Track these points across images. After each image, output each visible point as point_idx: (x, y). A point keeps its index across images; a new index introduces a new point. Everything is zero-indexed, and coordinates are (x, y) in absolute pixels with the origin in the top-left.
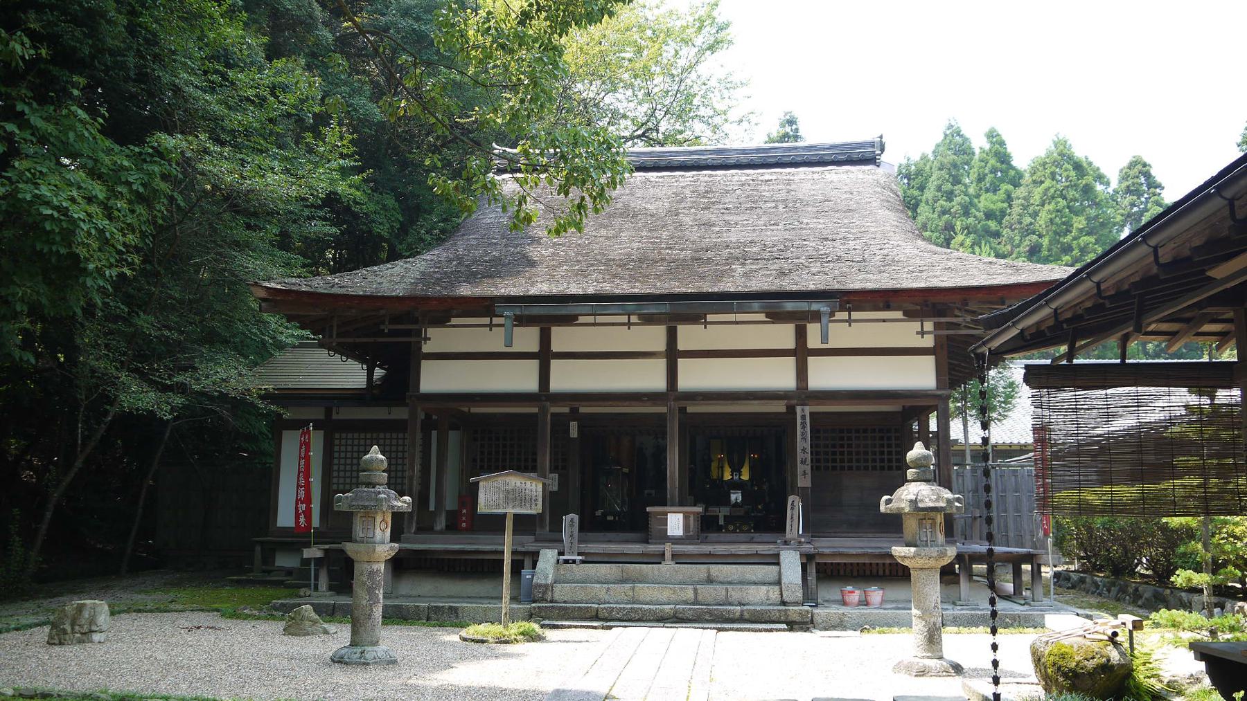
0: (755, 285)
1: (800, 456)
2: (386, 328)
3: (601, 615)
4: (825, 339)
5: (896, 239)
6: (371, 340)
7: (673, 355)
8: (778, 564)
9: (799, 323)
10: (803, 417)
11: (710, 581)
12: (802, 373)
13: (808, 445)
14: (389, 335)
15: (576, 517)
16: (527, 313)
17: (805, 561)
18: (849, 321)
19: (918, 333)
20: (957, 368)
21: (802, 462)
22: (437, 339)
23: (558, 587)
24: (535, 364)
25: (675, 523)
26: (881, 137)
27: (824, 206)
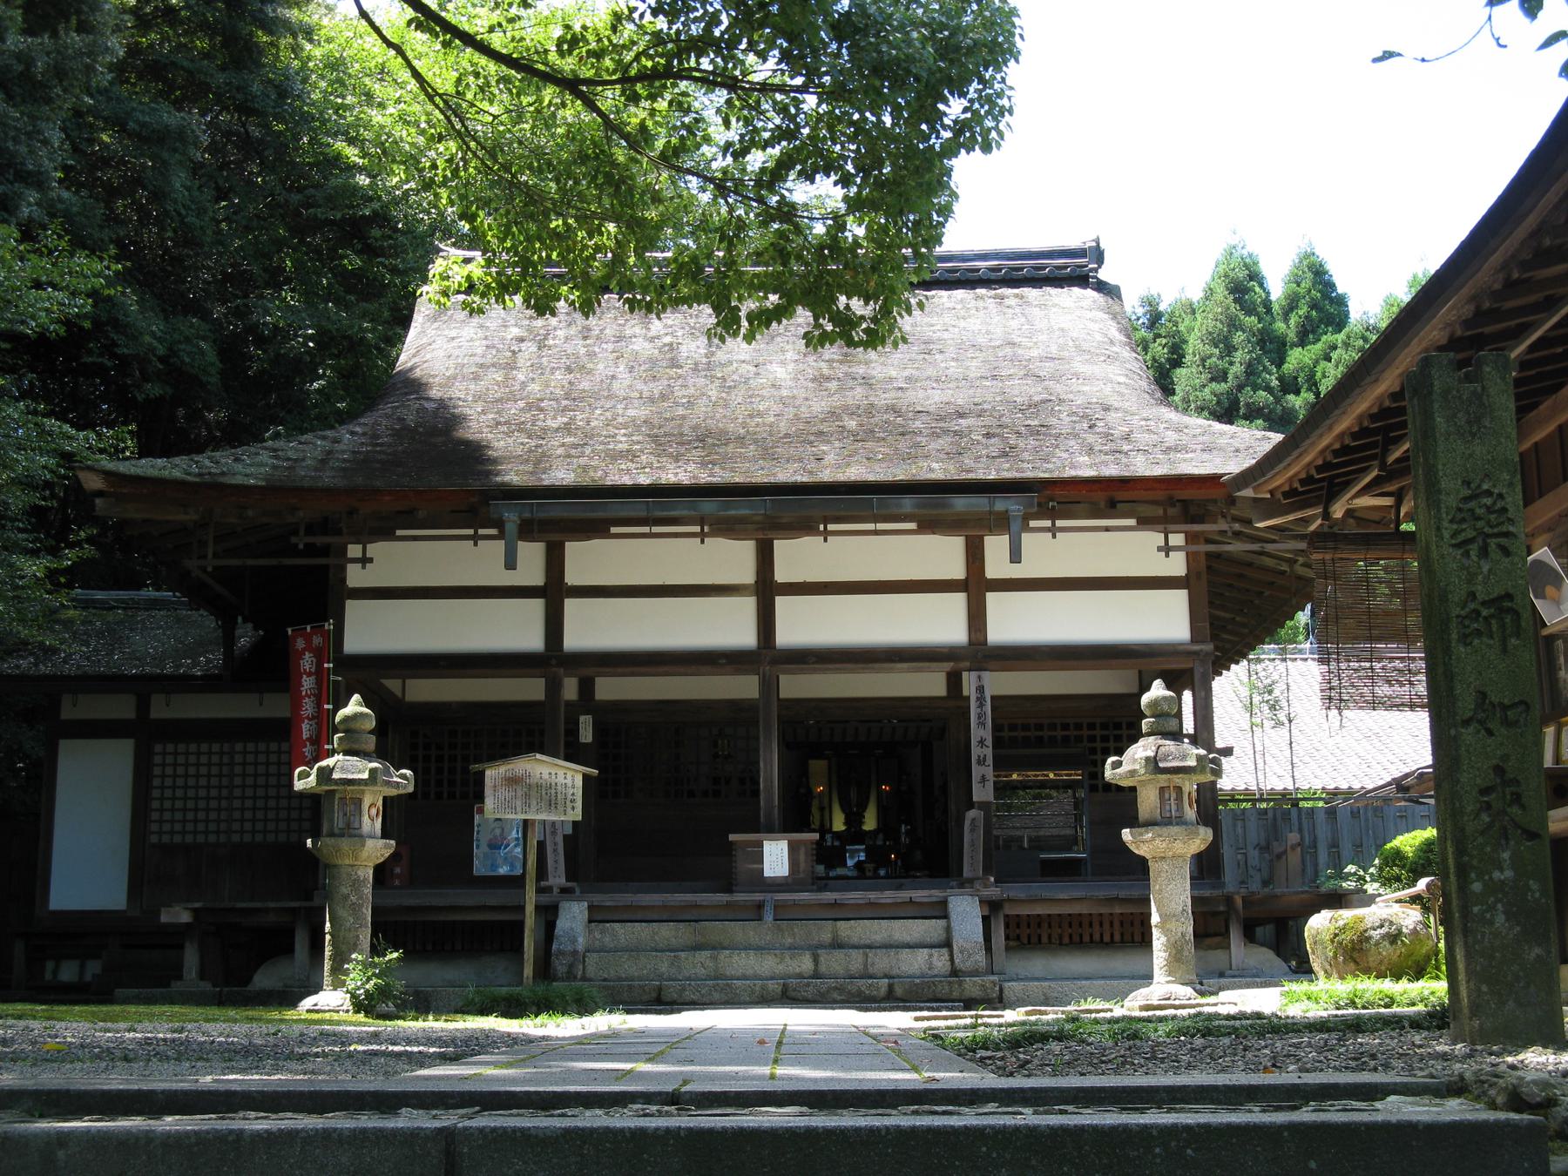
1: (976, 751)
2: (301, 542)
4: (1015, 557)
6: (273, 562)
7: (766, 590)
8: (946, 916)
11: (837, 945)
12: (977, 618)
16: (542, 515)
17: (986, 913)
18: (1053, 531)
19: (1159, 549)
20: (1230, 627)
21: (979, 762)
23: (592, 959)
25: (776, 857)
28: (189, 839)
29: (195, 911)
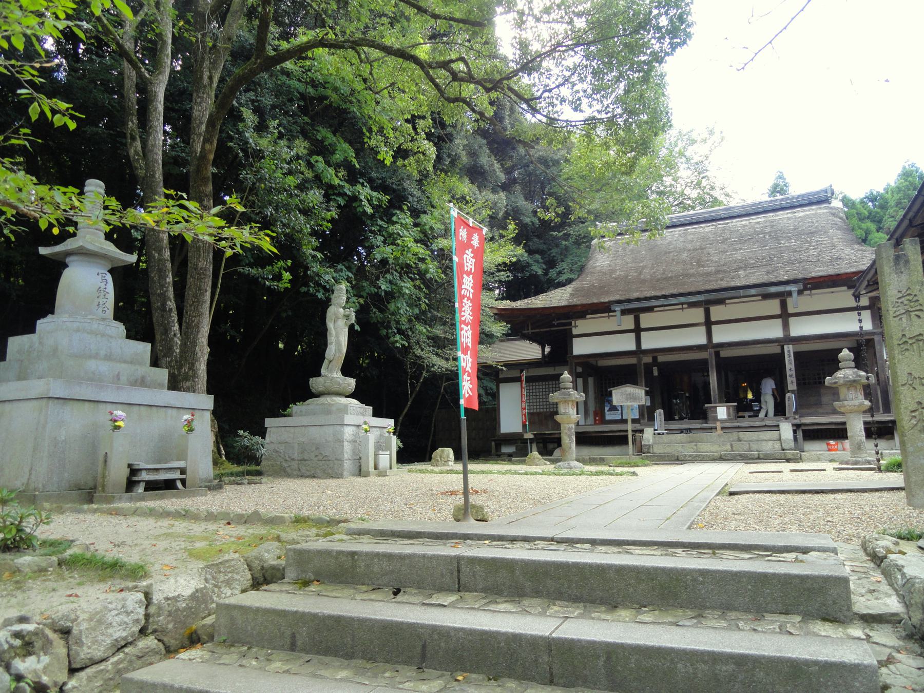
0: (752, 281)
1: (788, 373)
2: (555, 323)
3: (680, 459)
5: (840, 246)
7: (709, 324)
9: (637, 314)
10: (789, 351)
13: (793, 367)
14: (556, 326)
15: (662, 411)
22: (580, 326)
23: (655, 446)
24: (633, 335)
26: (831, 186)
27: (798, 233)
28: (538, 411)
29: (534, 434)
